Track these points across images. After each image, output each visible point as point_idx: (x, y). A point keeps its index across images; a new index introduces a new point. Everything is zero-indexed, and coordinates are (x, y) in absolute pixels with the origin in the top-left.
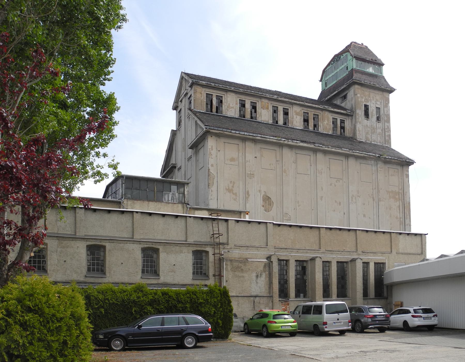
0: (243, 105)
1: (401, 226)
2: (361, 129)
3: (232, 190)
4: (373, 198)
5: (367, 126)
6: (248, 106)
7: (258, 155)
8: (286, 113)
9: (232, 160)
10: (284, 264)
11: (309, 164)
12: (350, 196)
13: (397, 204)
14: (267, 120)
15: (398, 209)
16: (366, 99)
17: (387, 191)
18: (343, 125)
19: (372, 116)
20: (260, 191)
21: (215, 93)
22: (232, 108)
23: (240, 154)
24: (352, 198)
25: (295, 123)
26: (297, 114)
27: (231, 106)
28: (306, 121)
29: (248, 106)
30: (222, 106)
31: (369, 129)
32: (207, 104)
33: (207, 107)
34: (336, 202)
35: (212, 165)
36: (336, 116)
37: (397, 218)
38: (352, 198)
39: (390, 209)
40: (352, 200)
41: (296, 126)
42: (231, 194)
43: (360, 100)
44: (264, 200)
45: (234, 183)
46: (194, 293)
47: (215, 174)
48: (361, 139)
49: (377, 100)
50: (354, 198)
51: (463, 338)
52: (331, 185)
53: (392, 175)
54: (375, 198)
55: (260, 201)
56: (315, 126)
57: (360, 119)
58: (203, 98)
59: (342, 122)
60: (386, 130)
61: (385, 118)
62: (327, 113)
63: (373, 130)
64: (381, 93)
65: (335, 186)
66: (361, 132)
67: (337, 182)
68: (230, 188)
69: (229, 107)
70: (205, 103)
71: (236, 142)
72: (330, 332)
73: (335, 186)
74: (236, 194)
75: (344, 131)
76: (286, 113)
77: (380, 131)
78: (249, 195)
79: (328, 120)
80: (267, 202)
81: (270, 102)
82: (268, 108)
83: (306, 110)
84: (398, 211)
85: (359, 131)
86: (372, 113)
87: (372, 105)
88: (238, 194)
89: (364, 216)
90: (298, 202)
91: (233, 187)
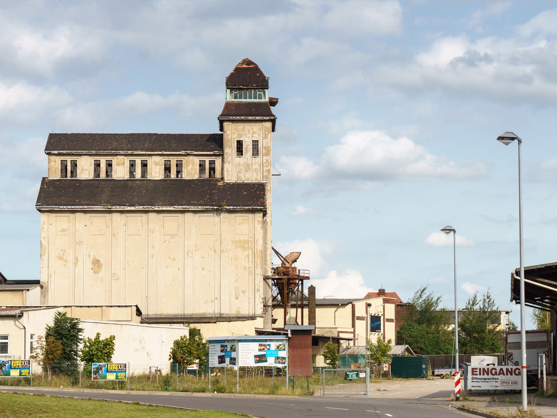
1: (250, 276)
2: (230, 169)
3: (63, 257)
4: (215, 250)
5: (239, 164)
7: (88, 223)
8: (144, 165)
9: (63, 230)
11: (141, 225)
12: (186, 250)
13: (246, 253)
14: (123, 176)
15: (247, 258)
17: (232, 241)
19: (247, 151)
20: (89, 256)
21: (69, 159)
22: (86, 170)
23: (71, 225)
24: (188, 253)
25: (153, 174)
26: (156, 164)
27: (85, 168)
28: (167, 169)
30: (76, 170)
31: (241, 167)
32: (62, 170)
33: (62, 173)
34: (169, 258)
35: (44, 238)
37: (245, 268)
38: (188, 253)
39: (236, 259)
40: (188, 255)
41: (155, 177)
42: (62, 261)
43: (230, 137)
44: (93, 263)
45: (65, 251)
47: (47, 246)
48: (229, 180)
49: (254, 133)
50: (190, 253)
51: (555, 406)
52: (165, 242)
53: (240, 224)
54: (217, 250)
55: (89, 264)
56: (178, 172)
57: (230, 158)
58: (58, 166)
59: (212, 163)
60: (264, 165)
61: (264, 151)
62: (191, 157)
63: (248, 167)
65: (169, 242)
66: (230, 173)
67: (171, 238)
68: (61, 255)
69: (82, 170)
70: (60, 170)
72: (351, 396)
73: (169, 242)
74: (66, 261)
75: (214, 173)
76: (144, 165)
77: (257, 166)
78: (78, 260)
79: (193, 165)
80: (96, 264)
81: (126, 158)
82: (124, 164)
83: (167, 158)
84: (247, 260)
85: (228, 171)
86: (247, 148)
87: (247, 139)
88: (68, 261)
89: (203, 269)
90: (128, 262)
91: (63, 254)
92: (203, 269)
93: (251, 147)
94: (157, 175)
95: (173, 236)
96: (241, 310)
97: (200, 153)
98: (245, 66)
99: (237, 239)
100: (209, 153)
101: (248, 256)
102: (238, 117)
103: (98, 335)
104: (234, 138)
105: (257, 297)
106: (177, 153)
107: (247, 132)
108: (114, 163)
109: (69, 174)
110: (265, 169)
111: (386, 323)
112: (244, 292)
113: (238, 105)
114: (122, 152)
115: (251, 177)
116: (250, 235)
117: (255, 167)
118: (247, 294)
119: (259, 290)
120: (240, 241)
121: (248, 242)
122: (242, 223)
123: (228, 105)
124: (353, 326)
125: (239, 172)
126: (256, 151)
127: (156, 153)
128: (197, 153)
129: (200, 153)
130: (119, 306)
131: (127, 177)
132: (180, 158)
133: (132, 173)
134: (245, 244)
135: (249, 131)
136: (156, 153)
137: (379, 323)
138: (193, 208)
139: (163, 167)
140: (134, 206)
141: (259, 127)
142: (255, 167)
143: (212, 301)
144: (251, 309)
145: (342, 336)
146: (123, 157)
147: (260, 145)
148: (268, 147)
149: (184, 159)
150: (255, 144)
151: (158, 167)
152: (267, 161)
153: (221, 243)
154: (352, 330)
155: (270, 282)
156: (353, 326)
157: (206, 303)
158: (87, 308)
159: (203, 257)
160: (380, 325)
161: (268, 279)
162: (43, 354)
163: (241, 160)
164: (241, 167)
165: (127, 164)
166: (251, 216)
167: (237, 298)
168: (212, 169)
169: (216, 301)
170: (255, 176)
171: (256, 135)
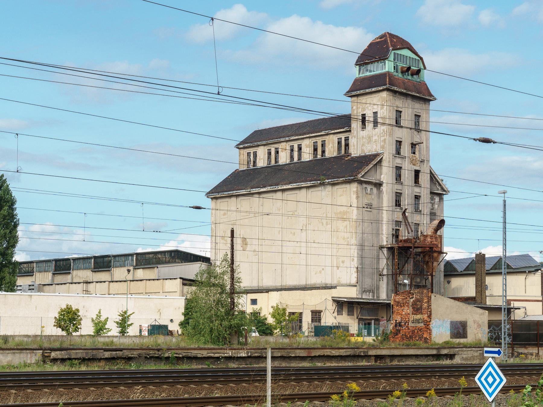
21: (251, 150)
26: (307, 146)
36: (340, 136)
48: (355, 154)
53: (341, 196)
62: (331, 136)
71: (227, 199)
77: (376, 138)
96: (341, 280)
97: (336, 131)
98: (379, 40)
100: (342, 130)
101: (346, 226)
103: (272, 307)
104: (359, 113)
106: (320, 134)
109: (252, 164)
114: (282, 139)
125: (363, 145)
127: (305, 136)
128: (333, 132)
129: (336, 131)
130: (171, 279)
131: (288, 161)
132: (324, 138)
133: (292, 157)
134: (344, 215)
136: (305, 136)
138: (304, 184)
139: (312, 149)
140: (265, 187)
141: (378, 98)
142: (375, 138)
143: (320, 272)
149: (326, 138)
155: (385, 251)
157: (316, 274)
161: (384, 248)
162: (123, 323)
164: (364, 140)
165: (288, 148)
166: (348, 186)
170: (375, 147)
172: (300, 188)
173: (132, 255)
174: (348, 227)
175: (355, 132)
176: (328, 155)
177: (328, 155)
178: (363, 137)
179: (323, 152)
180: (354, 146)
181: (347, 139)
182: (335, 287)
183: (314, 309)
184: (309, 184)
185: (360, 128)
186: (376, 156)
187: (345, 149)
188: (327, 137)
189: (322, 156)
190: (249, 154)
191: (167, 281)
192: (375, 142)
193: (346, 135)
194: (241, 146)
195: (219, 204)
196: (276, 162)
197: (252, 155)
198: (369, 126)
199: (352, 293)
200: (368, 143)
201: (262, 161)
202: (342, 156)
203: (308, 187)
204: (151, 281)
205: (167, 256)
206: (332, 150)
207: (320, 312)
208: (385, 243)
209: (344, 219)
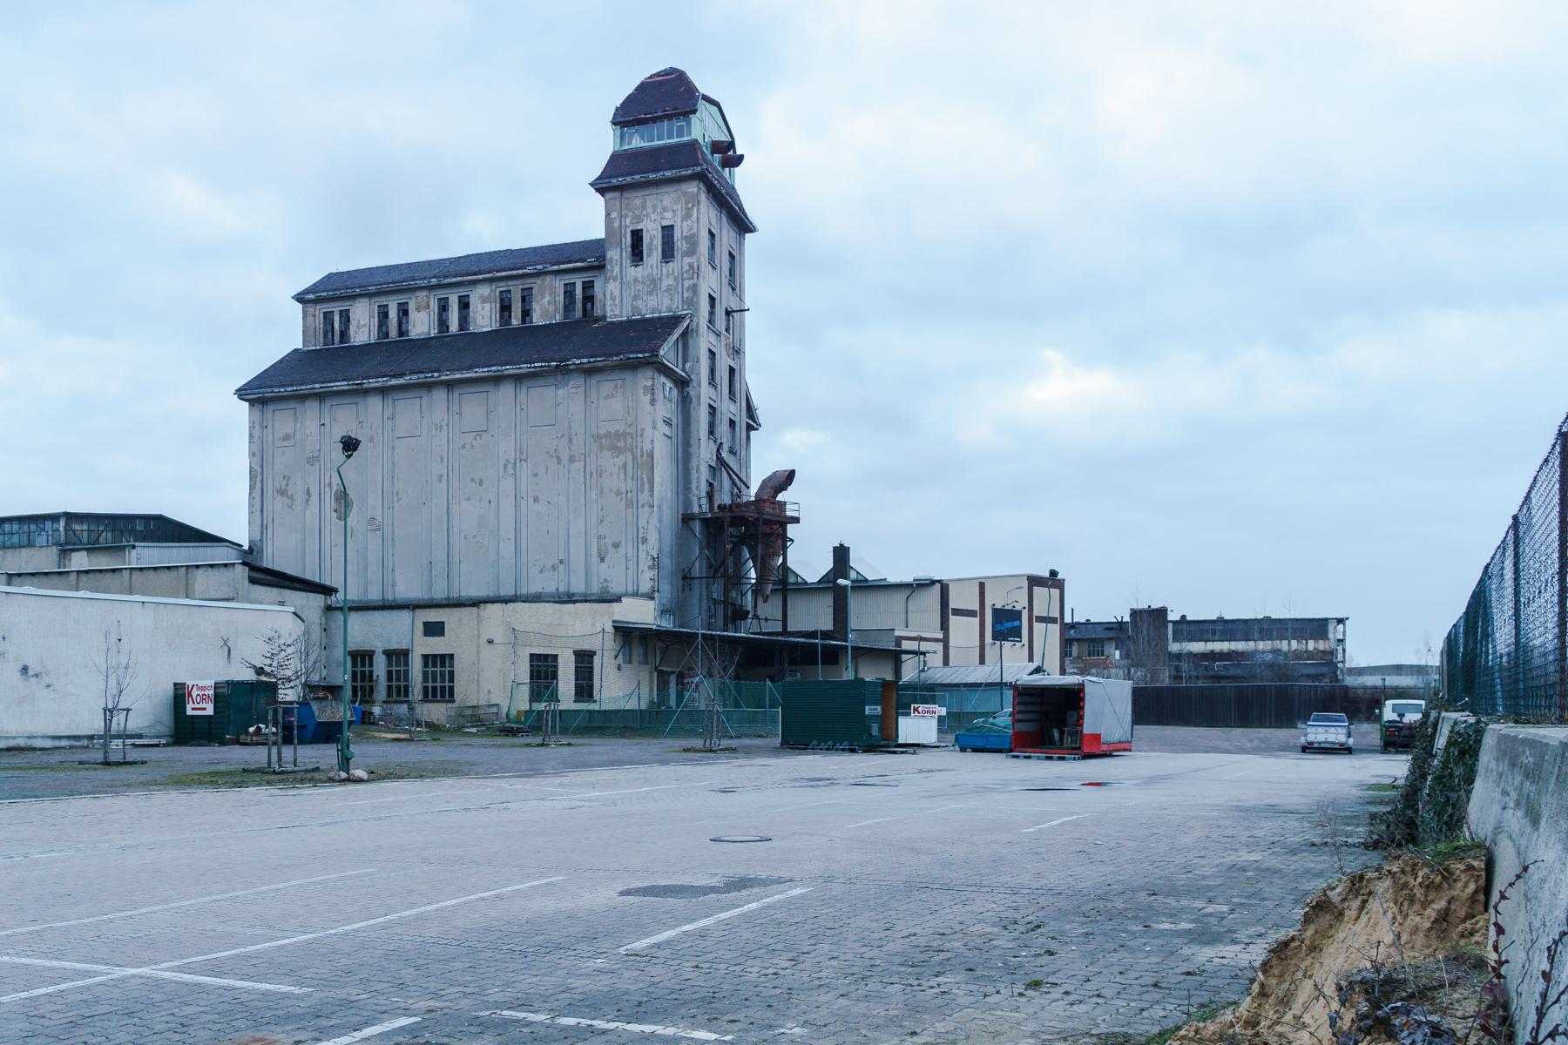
0: (384, 314)
5: (636, 280)
6: (393, 314)
9: (287, 437)
10: (1335, 632)
16: (635, 217)
18: (589, 293)
19: (650, 251)
21: (336, 308)
25: (479, 321)
26: (484, 300)
28: (505, 308)
29: (393, 314)
31: (639, 287)
36: (570, 278)
37: (618, 493)
46: (753, 719)
49: (665, 209)
50: (510, 467)
53: (608, 397)
59: (588, 286)
62: (548, 278)
64: (671, 189)
71: (293, 404)
74: (291, 497)
76: (464, 305)
77: (671, 281)
86: (651, 244)
89: (536, 500)
92: (536, 500)
93: (658, 242)
94: (487, 321)
95: (479, 434)
99: (602, 432)
101: (625, 466)
102: (629, 179)
105: (642, 555)
107: (650, 210)
108: (412, 307)
109: (337, 338)
110: (687, 283)
111: (1036, 625)
112: (616, 546)
113: (638, 154)
115: (656, 305)
116: (630, 421)
117: (666, 283)
118: (622, 550)
119: (645, 540)
120: (608, 435)
121: (625, 435)
122: (612, 396)
123: (615, 158)
124: (944, 626)
125: (636, 298)
126: (668, 253)
131: (434, 332)
132: (528, 283)
133: (443, 324)
135: (654, 206)
137: (1016, 623)
138: (510, 370)
142: (666, 283)
143: (554, 568)
144: (630, 581)
145: (906, 645)
146: (425, 293)
147: (677, 234)
148: (693, 236)
149: (536, 284)
150: (668, 231)
151: (487, 306)
152: (691, 266)
153: (570, 440)
154: (940, 636)
155: (697, 527)
156: (944, 626)
158: (152, 574)
159: (535, 475)
160: (1020, 628)
163: (634, 272)
164: (639, 287)
165: (434, 306)
167: (602, 560)
168: (589, 299)
169: (561, 567)
170: (667, 302)
171: (668, 215)
172: (497, 380)
173: (54, 518)
174: (629, 468)
175: (617, 269)
176: (538, 319)
177: (538, 319)
178: (636, 280)
179: (526, 314)
180: (613, 298)
181: (588, 286)
182: (618, 599)
183: (580, 648)
184: (525, 368)
185: (627, 262)
186: (675, 320)
187: (584, 309)
188: (538, 281)
189: (524, 321)
190: (328, 316)
191: (200, 572)
192: (667, 290)
193: (587, 277)
194: (312, 296)
195: (270, 414)
196: (401, 333)
197: (337, 318)
198: (653, 256)
199: (642, 613)
200: (650, 293)
201: (366, 330)
202: (578, 322)
203: (518, 379)
204: (146, 573)
205: (139, 527)
206: (551, 308)
207: (591, 654)
208: (696, 510)
209: (617, 451)
